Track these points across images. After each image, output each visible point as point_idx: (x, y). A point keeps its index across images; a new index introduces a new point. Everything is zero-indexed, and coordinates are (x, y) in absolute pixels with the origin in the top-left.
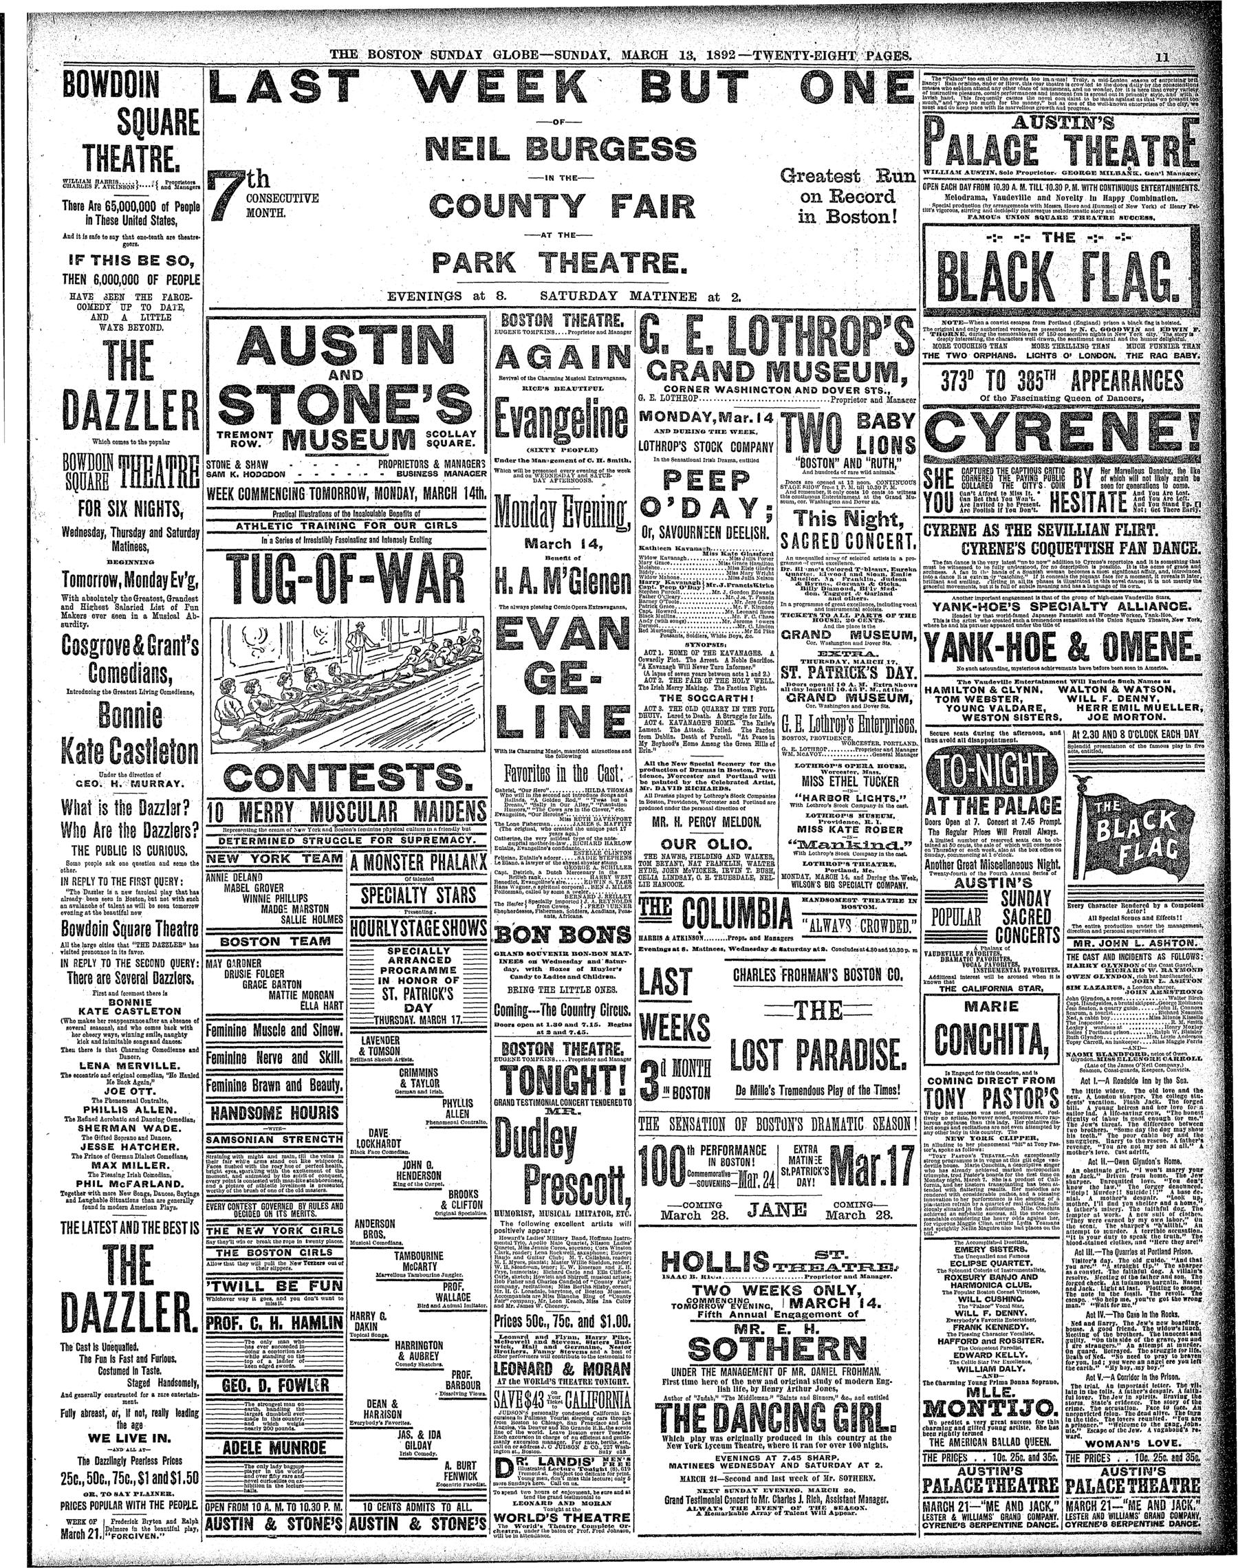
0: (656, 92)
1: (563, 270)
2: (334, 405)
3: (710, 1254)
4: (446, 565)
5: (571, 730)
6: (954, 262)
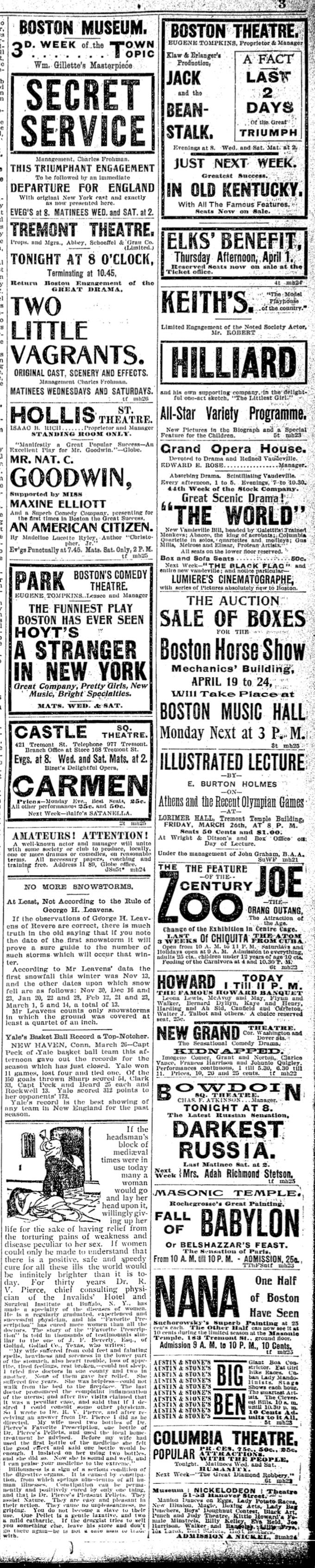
2: (42, 415)
3: (48, 409)
4: (232, 1215)
5: (295, 1088)
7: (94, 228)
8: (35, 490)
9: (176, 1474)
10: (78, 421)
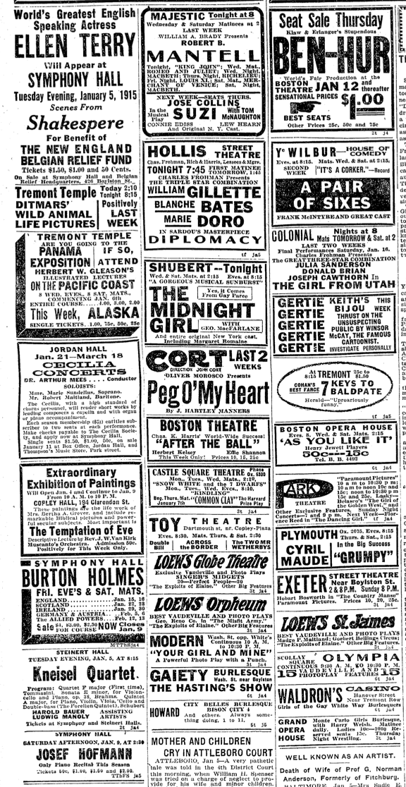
0: (206, 209)
1: (281, 288)
3: (174, 147)
6: (109, 38)
7: (204, 444)
8: (213, 229)
9: (102, 723)
10: (193, 155)
